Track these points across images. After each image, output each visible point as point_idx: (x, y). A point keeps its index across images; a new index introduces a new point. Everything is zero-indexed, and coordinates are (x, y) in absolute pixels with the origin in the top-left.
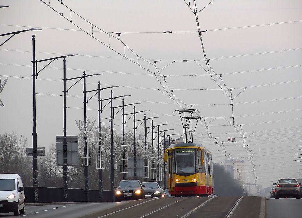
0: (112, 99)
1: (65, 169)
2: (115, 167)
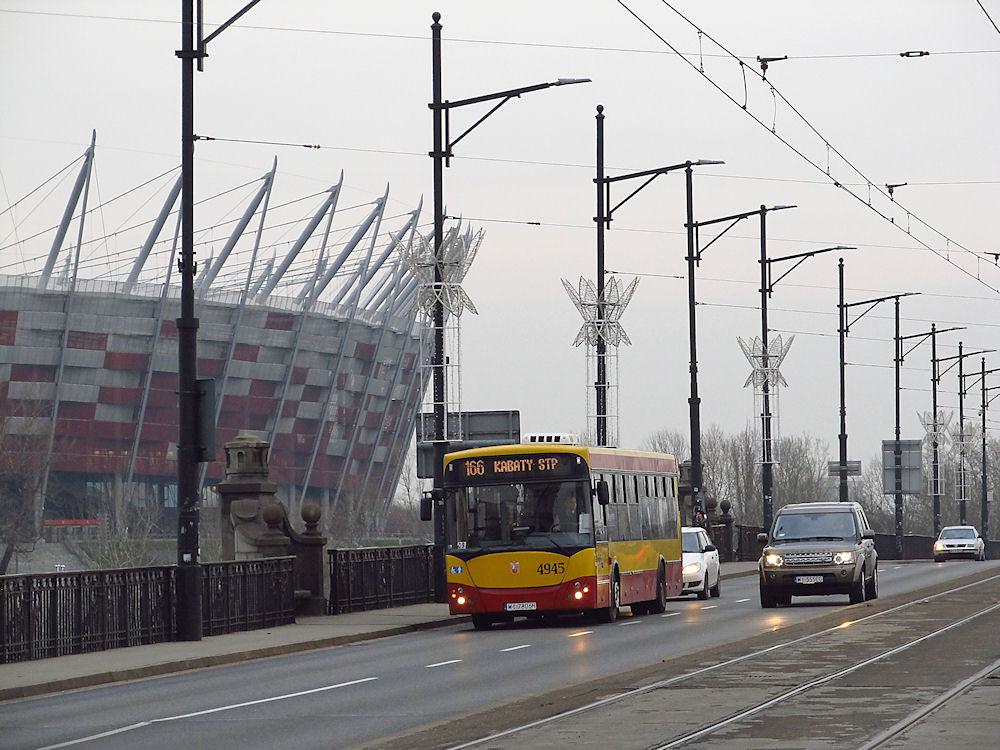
1: (899, 501)
2: (990, 498)
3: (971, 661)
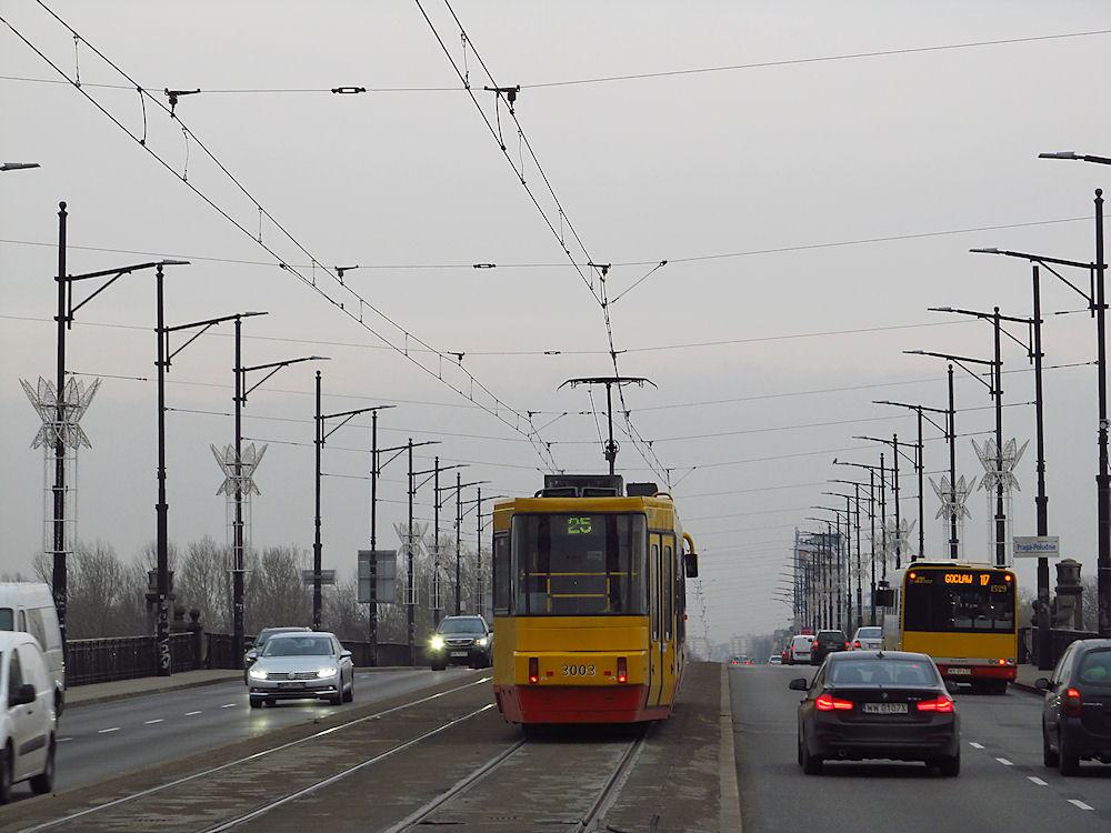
0: (459, 487)
1: (373, 609)
3: (407, 798)
